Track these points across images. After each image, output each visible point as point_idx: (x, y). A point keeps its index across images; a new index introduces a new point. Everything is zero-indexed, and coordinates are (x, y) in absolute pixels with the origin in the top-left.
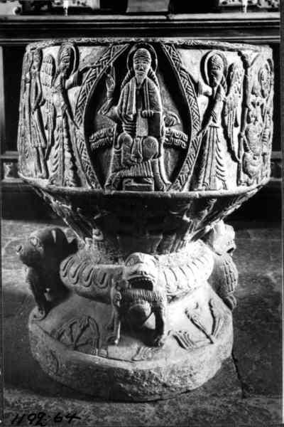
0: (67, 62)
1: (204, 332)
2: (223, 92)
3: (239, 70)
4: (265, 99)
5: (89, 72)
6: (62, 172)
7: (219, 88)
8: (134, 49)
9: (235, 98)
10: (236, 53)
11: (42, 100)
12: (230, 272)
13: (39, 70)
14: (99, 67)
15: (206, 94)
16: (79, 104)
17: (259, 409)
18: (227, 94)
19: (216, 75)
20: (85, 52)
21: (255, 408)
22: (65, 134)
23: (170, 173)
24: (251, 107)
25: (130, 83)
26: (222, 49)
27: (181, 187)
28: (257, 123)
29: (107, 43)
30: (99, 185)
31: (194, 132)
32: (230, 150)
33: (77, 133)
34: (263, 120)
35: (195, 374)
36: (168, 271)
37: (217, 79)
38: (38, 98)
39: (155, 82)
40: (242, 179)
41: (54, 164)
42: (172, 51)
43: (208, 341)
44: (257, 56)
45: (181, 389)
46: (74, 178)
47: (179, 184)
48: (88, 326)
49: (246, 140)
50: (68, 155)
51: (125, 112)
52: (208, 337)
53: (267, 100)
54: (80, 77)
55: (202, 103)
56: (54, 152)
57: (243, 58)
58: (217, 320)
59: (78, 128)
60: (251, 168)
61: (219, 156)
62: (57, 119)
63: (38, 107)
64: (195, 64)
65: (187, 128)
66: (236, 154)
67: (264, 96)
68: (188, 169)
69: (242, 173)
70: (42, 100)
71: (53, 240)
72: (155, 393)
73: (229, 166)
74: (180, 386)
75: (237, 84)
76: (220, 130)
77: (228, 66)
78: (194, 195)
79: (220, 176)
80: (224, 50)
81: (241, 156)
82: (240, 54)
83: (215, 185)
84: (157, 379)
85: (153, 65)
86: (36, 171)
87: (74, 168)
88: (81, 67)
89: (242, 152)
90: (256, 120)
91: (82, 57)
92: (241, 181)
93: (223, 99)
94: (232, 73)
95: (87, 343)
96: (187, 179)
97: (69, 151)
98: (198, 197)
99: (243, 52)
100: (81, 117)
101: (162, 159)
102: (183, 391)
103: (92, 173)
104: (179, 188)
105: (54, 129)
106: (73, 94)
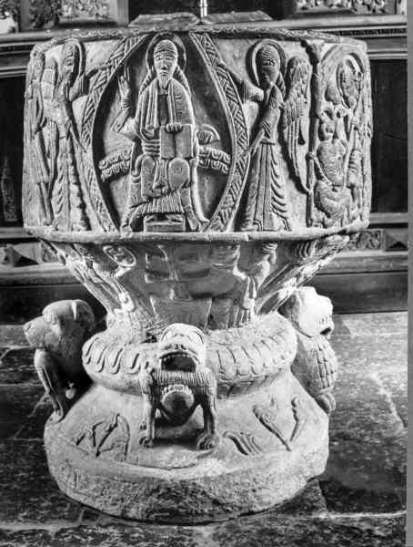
0: (70, 64)
2: (279, 95)
3: (304, 64)
5: (97, 75)
7: (273, 91)
8: (154, 40)
9: (299, 101)
10: (299, 43)
11: (43, 120)
12: (325, 361)
13: (40, 80)
14: (110, 67)
15: (255, 99)
16: (86, 118)
17: (348, 528)
18: (285, 99)
19: (270, 73)
20: (92, 49)
21: (342, 526)
22: (70, 160)
23: (207, 207)
24: (325, 117)
25: (150, 87)
26: (277, 37)
27: (222, 226)
28: (338, 141)
29: (120, 35)
30: (113, 226)
31: (238, 151)
32: (294, 177)
33: (85, 158)
35: (260, 488)
37: (271, 79)
38: (39, 116)
39: (184, 86)
40: (313, 216)
41: (58, 203)
43: (284, 447)
44: (332, 48)
45: (240, 508)
46: (82, 219)
47: (220, 221)
48: (116, 425)
49: (318, 163)
50: (74, 188)
51: (144, 125)
52: (284, 443)
53: (354, 111)
55: (249, 110)
56: (57, 186)
57: (309, 50)
59: (85, 152)
60: (327, 202)
62: (61, 141)
63: (39, 129)
64: (240, 58)
65: (227, 145)
66: (304, 183)
67: (348, 105)
68: (230, 201)
69: (313, 208)
70: (43, 120)
71: (72, 315)
72: (203, 514)
74: (239, 504)
75: (301, 85)
76: (277, 149)
77: (287, 61)
78: (241, 236)
79: (280, 212)
80: (279, 40)
81: (312, 185)
82: (304, 44)
83: (272, 224)
85: (181, 61)
86: (40, 217)
87: (83, 206)
88: (88, 69)
89: (314, 179)
90: (335, 136)
91: (89, 56)
92: (312, 221)
93: (279, 105)
95: (112, 448)
96: (230, 214)
97: (75, 184)
98: (247, 240)
99: (309, 42)
100: (88, 136)
101: (196, 187)
102: (243, 511)
103: (104, 210)
104: (219, 228)
105: (57, 155)
106: (79, 106)
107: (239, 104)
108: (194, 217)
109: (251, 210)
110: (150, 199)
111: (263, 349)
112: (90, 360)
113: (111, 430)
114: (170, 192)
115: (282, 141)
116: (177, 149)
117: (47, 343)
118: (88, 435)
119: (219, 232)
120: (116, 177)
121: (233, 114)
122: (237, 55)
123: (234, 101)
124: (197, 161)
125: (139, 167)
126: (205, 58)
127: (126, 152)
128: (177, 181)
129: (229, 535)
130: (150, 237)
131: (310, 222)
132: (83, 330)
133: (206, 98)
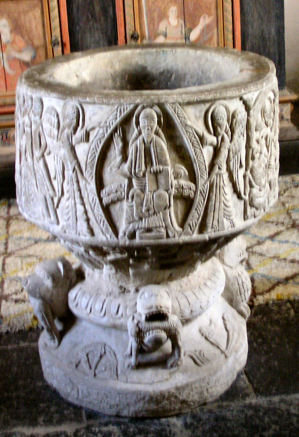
1: (218, 347)
2: (227, 139)
3: (242, 114)
4: (269, 129)
6: (75, 223)
10: (238, 99)
20: (89, 110)
30: (113, 236)
31: (201, 182)
34: (268, 151)
36: (180, 296)
42: (177, 109)
47: (189, 229)
50: (80, 208)
54: (87, 135)
55: (208, 152)
57: (245, 103)
58: (231, 333)
59: (89, 184)
61: (225, 199)
64: (200, 117)
65: (193, 177)
69: (248, 207)
73: (235, 205)
75: (240, 129)
76: (226, 176)
79: (228, 216)
84: (176, 397)
85: (159, 123)
87: (88, 220)
94: (234, 121)
99: (245, 97)
101: (172, 208)
107: (200, 149)
108: (172, 229)
109: (210, 221)
110: (141, 219)
111: (206, 290)
112: (77, 305)
113: (101, 357)
114: (155, 213)
115: (229, 169)
116: (159, 184)
117: (42, 294)
118: (82, 362)
119: (189, 237)
120: (113, 202)
121: (197, 158)
122: (198, 115)
123: (197, 148)
124: (173, 191)
125: (133, 197)
126: (177, 121)
127: (121, 186)
128: (159, 207)
129: (195, 423)
130: (142, 243)
131: (246, 217)
132: (68, 283)
133: (177, 146)
